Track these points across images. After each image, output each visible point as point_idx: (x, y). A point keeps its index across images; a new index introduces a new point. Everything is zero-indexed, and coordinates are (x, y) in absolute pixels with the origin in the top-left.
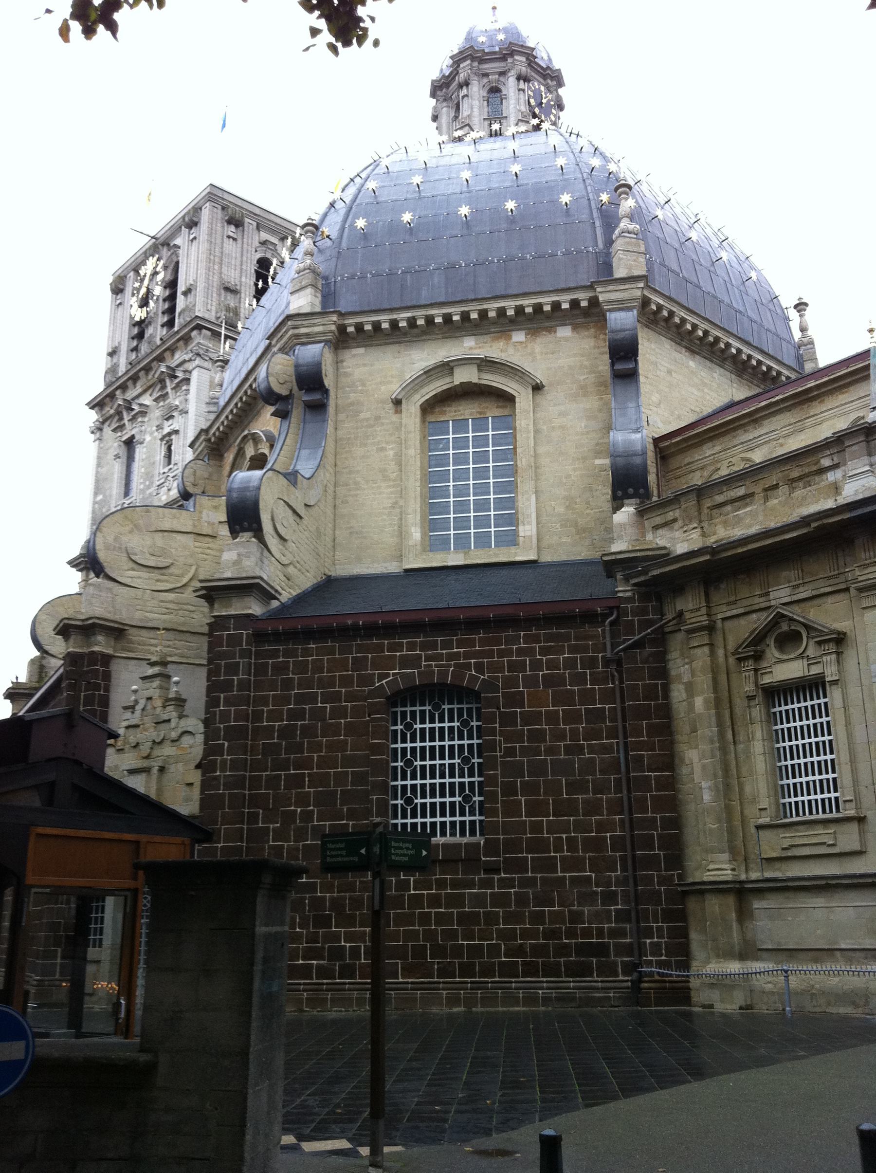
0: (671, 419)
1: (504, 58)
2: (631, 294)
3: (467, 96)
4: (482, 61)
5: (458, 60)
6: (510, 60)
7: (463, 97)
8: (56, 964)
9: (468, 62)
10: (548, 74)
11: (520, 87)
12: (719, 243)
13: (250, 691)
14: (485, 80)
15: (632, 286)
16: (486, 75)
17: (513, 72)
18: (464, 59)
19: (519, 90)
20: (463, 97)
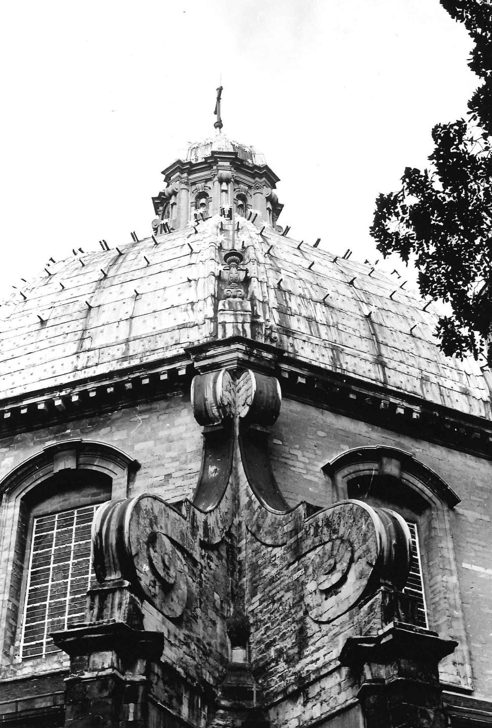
0: (438, 297)
1: (210, 167)
2: (398, 444)
3: (175, 204)
4: (190, 172)
5: (168, 175)
6: (215, 167)
7: (172, 205)
8: (51, 616)
9: (178, 174)
10: (256, 172)
11: (223, 189)
12: (199, 150)
13: (52, 598)
14: (194, 188)
15: (328, 713)
16: (194, 184)
17: (216, 179)
18: (173, 172)
19: (223, 191)
20: (172, 205)
